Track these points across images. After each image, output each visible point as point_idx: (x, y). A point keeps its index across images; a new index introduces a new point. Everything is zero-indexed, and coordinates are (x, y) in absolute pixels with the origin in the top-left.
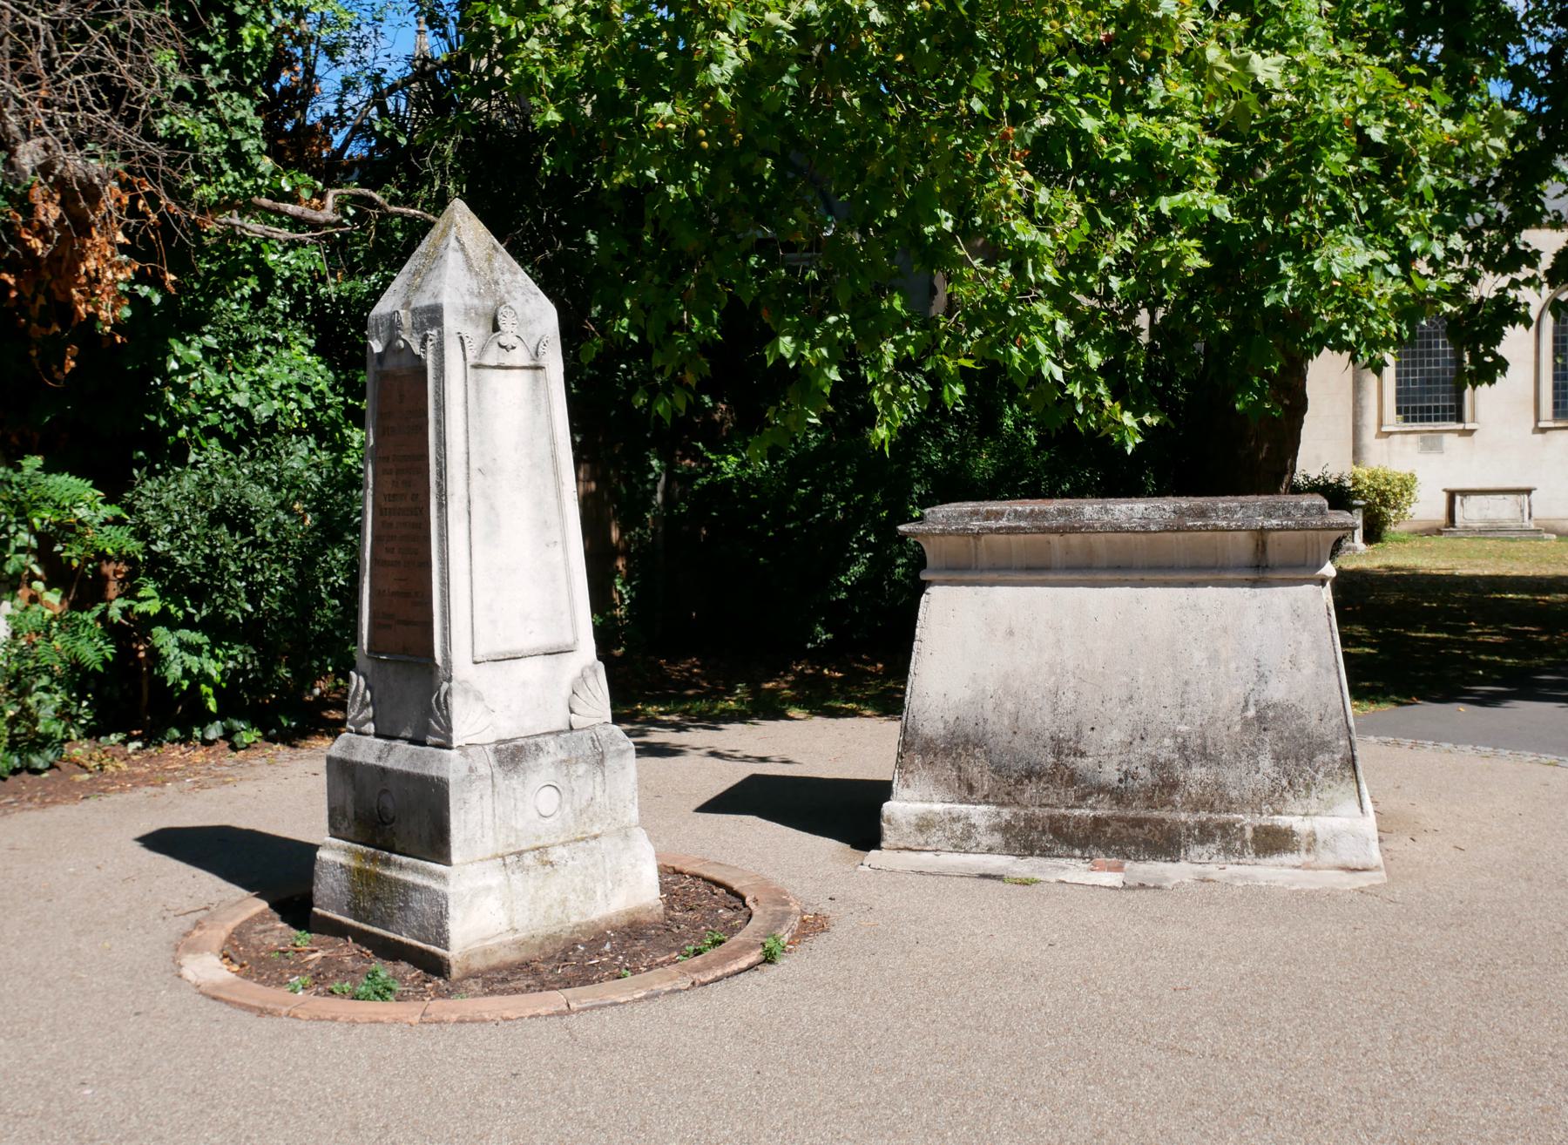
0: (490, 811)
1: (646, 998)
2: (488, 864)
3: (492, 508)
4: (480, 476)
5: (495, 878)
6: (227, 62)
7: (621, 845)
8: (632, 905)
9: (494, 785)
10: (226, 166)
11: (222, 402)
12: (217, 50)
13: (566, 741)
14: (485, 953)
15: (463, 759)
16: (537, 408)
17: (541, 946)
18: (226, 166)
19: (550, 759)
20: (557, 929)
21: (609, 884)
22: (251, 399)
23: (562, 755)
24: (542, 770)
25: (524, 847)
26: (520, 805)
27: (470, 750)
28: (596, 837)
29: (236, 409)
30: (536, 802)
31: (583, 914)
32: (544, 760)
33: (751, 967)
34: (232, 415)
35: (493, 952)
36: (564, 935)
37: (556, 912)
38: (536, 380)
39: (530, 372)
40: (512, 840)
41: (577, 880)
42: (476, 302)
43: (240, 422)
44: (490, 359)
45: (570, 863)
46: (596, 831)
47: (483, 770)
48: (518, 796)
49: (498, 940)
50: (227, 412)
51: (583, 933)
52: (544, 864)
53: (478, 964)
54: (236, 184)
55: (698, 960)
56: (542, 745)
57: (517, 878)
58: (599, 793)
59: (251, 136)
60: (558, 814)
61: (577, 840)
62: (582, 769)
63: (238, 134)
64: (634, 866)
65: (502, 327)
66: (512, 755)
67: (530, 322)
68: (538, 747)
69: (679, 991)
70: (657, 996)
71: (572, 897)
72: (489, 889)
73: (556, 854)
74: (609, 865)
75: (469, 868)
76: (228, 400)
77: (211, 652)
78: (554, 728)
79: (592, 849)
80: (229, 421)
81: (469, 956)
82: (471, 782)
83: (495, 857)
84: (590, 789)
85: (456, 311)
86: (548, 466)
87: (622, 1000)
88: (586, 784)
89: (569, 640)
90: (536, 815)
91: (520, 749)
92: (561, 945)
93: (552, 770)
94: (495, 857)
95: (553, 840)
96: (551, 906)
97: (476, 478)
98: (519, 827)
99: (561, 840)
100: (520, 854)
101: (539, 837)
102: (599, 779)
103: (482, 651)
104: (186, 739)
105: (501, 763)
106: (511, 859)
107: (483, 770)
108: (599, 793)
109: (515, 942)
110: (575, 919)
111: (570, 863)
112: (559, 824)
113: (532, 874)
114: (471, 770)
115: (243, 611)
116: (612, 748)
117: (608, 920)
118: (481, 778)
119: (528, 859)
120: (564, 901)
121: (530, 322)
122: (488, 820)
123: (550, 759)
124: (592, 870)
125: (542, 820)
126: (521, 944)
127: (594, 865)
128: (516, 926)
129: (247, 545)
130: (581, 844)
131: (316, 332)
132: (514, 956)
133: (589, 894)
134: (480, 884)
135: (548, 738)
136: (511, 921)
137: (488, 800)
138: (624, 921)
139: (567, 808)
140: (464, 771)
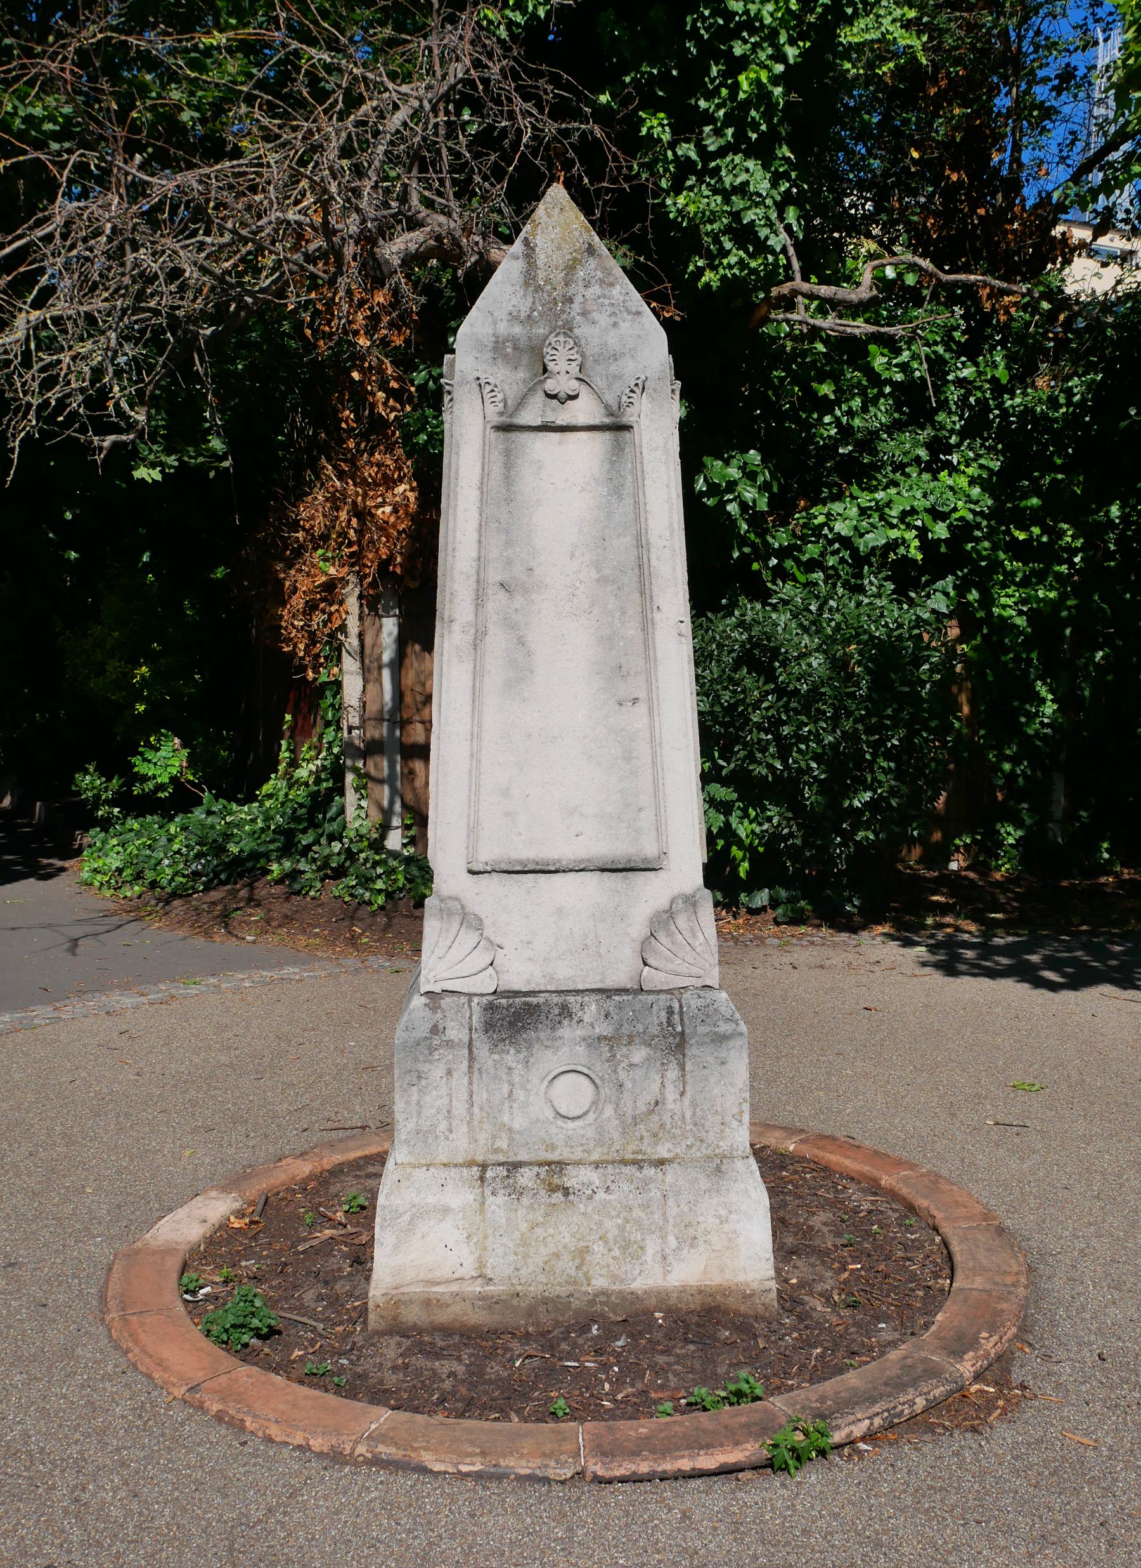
0: (465, 1096)
1: (478, 1476)
2: (453, 1172)
3: (521, 642)
4: (502, 595)
5: (460, 1195)
6: (728, 121)
7: (704, 1183)
8: (715, 1279)
9: (472, 1058)
10: (728, 245)
11: (826, 531)
12: (719, 107)
13: (620, 1007)
14: (427, 1303)
15: (427, 1013)
16: (617, 491)
17: (531, 1312)
18: (728, 245)
19: (580, 1032)
20: (563, 1291)
21: (672, 1242)
22: (856, 528)
23: (604, 1029)
24: (566, 1047)
25: (523, 1156)
26: (519, 1094)
27: (446, 1002)
28: (661, 1163)
29: (839, 538)
30: (553, 1094)
31: (615, 1278)
32: (567, 1031)
33: (726, 1471)
34: (837, 545)
35: (441, 1304)
36: (576, 1304)
37: (567, 1265)
38: (618, 449)
39: (607, 436)
40: (503, 1144)
41: (608, 1224)
42: (517, 330)
43: (846, 554)
44: (530, 416)
45: (601, 1195)
46: (663, 1152)
47: (456, 1032)
48: (516, 1079)
49: (454, 1288)
50: (831, 542)
51: (614, 1308)
52: (553, 1189)
53: (412, 1315)
54: (741, 263)
55: (687, 1421)
56: (575, 1007)
57: (497, 1204)
58: (671, 1094)
59: (757, 205)
60: (591, 1117)
61: (624, 1162)
62: (639, 1054)
63: (738, 202)
64: (723, 1221)
65: (551, 366)
66: (515, 1017)
67: (615, 357)
68: (565, 1011)
69: (546, 1480)
70: (499, 1477)
71: (598, 1248)
72: (446, 1210)
73: (574, 1178)
74: (672, 1211)
75: (420, 1174)
76: (831, 530)
77: (745, 811)
78: (609, 983)
79: (647, 1182)
80: (833, 553)
81: (397, 1302)
82: (431, 1050)
83: (470, 1164)
84: (655, 1087)
85: (480, 346)
86: (630, 579)
87: (437, 1467)
88: (647, 1079)
89: (649, 849)
90: (550, 1114)
91: (532, 1011)
92: (568, 1317)
93: (581, 1049)
94: (470, 1164)
95: (578, 1155)
96: (557, 1255)
97: (496, 600)
98: (516, 1126)
99: (595, 1156)
100: (516, 1166)
101: (552, 1147)
102: (673, 1073)
103: (487, 855)
104: (716, 904)
105: (489, 1026)
106: (496, 1172)
107: (456, 1032)
108: (671, 1094)
109: (482, 1297)
110: (600, 1283)
111: (601, 1195)
112: (591, 1133)
113: (525, 1201)
114: (435, 1030)
115: (771, 767)
116: (702, 1029)
117: (662, 1298)
118: (449, 1044)
119: (526, 1177)
120: (582, 1253)
121: (615, 357)
122: (460, 1108)
123: (580, 1032)
124: (637, 1213)
125: (560, 1122)
126: (491, 1302)
127: (645, 1206)
128: (489, 1272)
129: (772, 692)
130: (628, 1170)
131: (1003, 452)
132: (478, 1317)
133: (631, 1249)
134: (431, 1200)
135: (594, 997)
136: (481, 1264)
137: (460, 1081)
138: (696, 1303)
139: (609, 1111)
140: (423, 1030)
